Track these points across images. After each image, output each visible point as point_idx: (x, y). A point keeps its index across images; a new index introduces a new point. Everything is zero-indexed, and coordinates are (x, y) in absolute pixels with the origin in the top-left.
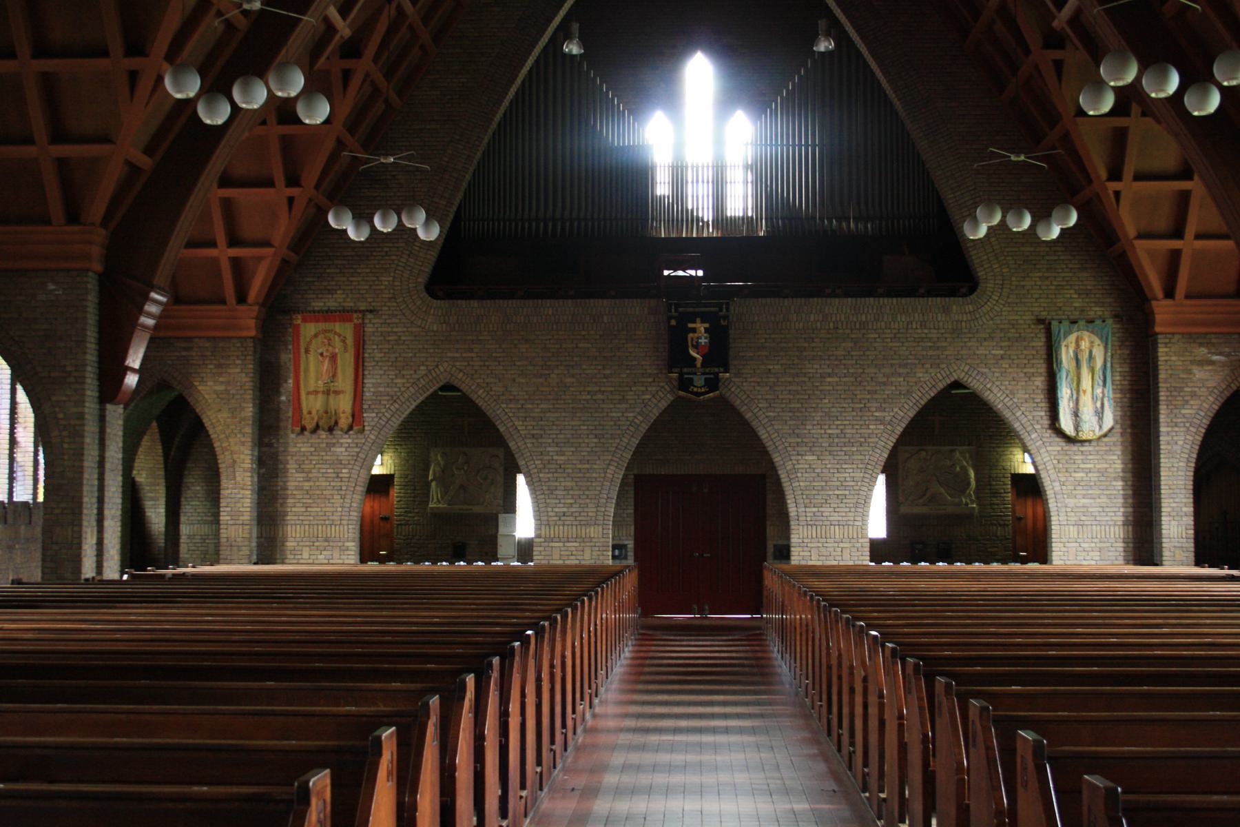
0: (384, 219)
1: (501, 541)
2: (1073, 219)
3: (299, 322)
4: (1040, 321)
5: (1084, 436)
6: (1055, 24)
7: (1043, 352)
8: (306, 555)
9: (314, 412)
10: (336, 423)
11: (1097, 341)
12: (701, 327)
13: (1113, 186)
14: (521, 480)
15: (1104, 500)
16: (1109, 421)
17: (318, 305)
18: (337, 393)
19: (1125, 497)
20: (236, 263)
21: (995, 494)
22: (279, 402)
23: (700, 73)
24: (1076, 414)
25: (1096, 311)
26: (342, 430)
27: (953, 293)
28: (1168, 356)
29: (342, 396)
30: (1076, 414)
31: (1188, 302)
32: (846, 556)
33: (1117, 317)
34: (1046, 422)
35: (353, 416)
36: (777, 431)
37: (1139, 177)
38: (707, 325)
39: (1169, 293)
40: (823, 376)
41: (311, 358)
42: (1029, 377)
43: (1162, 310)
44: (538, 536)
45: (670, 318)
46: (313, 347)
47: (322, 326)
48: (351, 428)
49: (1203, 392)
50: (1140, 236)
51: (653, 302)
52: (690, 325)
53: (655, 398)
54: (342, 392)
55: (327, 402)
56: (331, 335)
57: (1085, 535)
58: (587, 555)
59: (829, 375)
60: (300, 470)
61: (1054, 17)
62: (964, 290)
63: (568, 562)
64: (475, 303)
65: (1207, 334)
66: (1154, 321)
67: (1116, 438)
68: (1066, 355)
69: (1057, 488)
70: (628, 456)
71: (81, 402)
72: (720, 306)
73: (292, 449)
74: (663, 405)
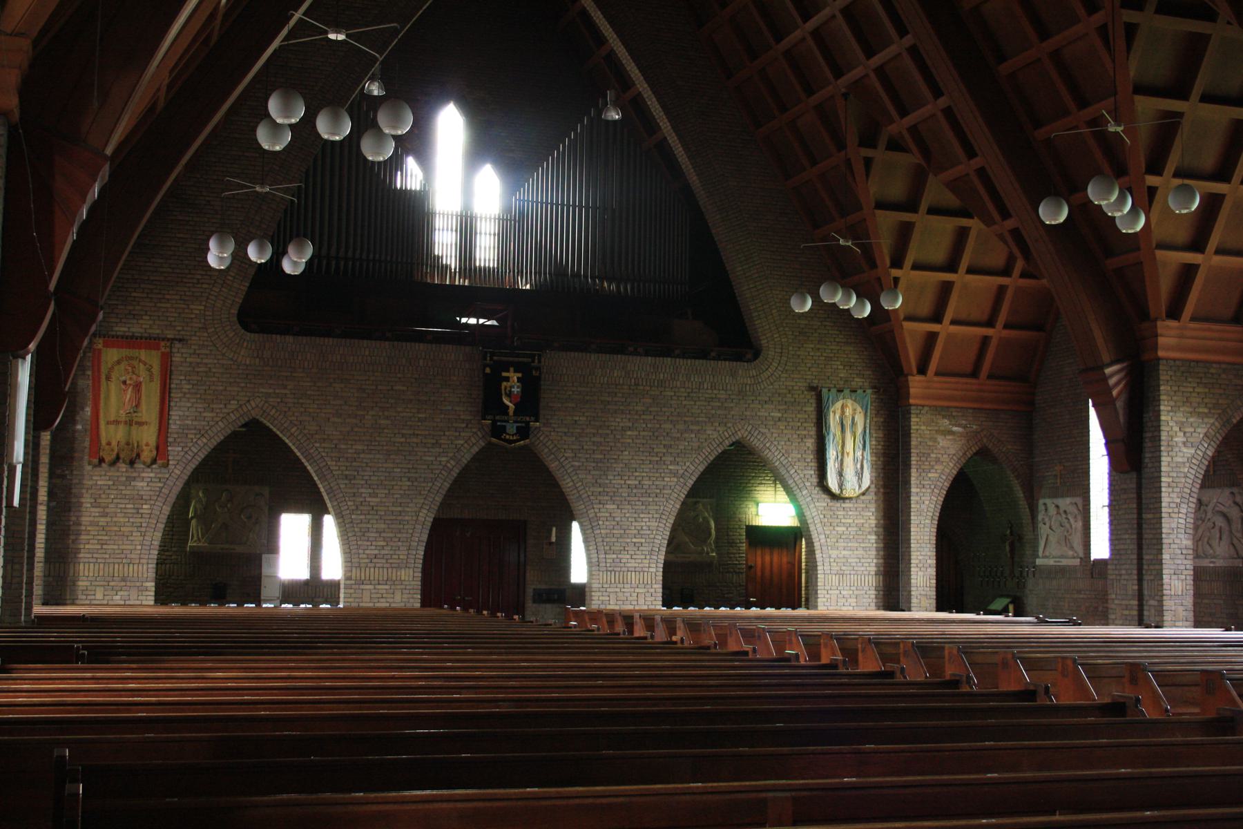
1: (264, 581)
3: (100, 346)
4: (812, 388)
5: (846, 494)
7: (813, 416)
8: (99, 596)
9: (114, 443)
10: (138, 455)
11: (859, 409)
12: (514, 376)
13: (895, 272)
14: (575, 526)
15: (861, 552)
16: (866, 482)
17: (121, 329)
18: (140, 424)
19: (877, 549)
21: (732, 543)
22: (75, 431)
23: (450, 124)
24: (841, 474)
25: (858, 382)
26: (144, 463)
27: (739, 358)
28: (920, 426)
29: (145, 427)
30: (841, 474)
31: (936, 379)
32: (641, 601)
34: (815, 480)
35: (157, 448)
36: (581, 480)
37: (916, 267)
38: (520, 375)
39: (922, 370)
40: (624, 430)
41: (113, 386)
42: (802, 438)
43: (916, 385)
44: (347, 578)
45: (485, 366)
46: (114, 376)
47: (125, 352)
48: (154, 461)
49: (945, 458)
51: (468, 349)
52: (504, 374)
53: (464, 443)
54: (146, 423)
55: (129, 433)
56: (135, 363)
57: (844, 588)
58: (398, 597)
59: (630, 429)
60: (96, 504)
62: (749, 356)
63: (377, 605)
64: (290, 339)
65: (948, 407)
66: (908, 395)
67: (871, 496)
68: (833, 420)
69: (823, 541)
70: (439, 499)
72: (533, 356)
73: (88, 483)
74: (476, 449)
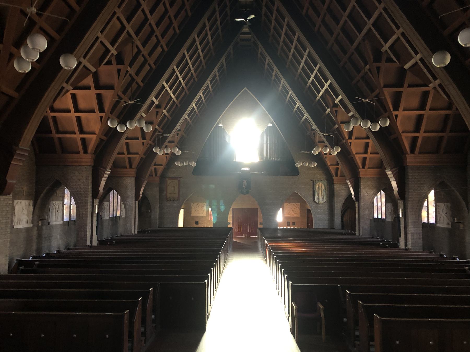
0: (186, 163)
2: (340, 150)
6: (335, 102)
13: (349, 141)
16: (325, 200)
20: (83, 140)
33: (327, 180)
39: (337, 176)
43: (335, 179)
50: (356, 154)
61: (383, 46)
68: (317, 187)
71: (87, 197)
